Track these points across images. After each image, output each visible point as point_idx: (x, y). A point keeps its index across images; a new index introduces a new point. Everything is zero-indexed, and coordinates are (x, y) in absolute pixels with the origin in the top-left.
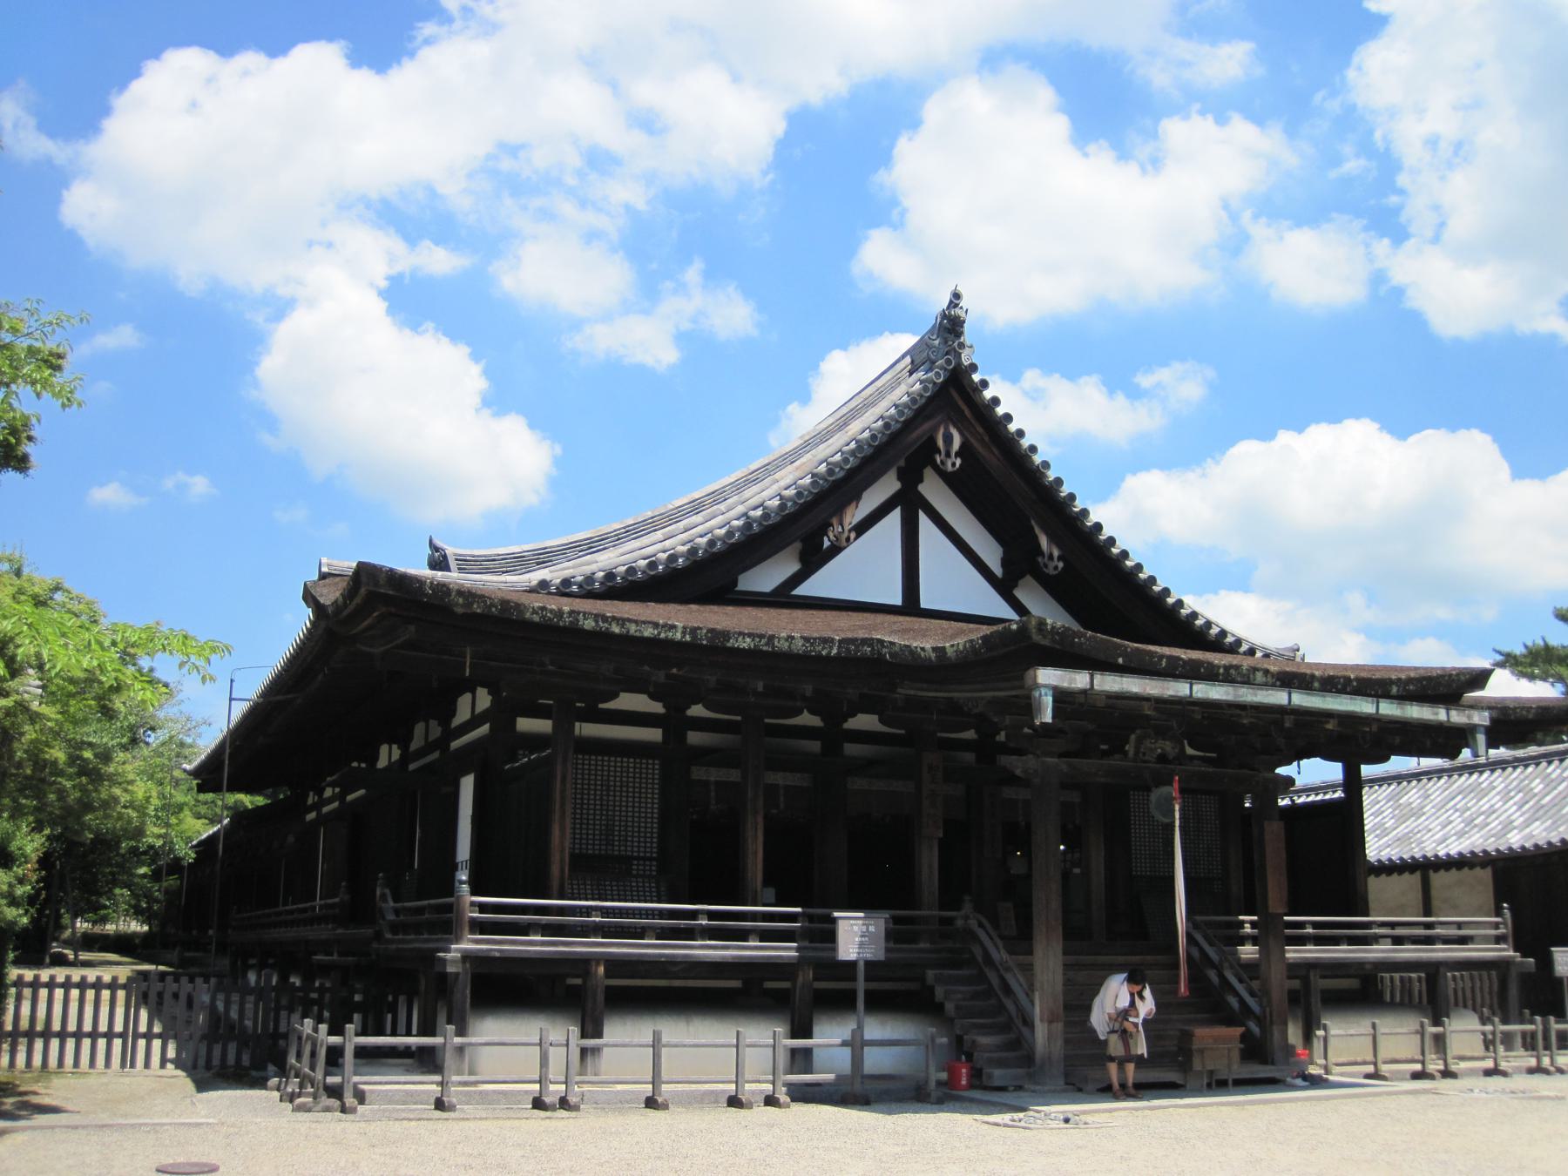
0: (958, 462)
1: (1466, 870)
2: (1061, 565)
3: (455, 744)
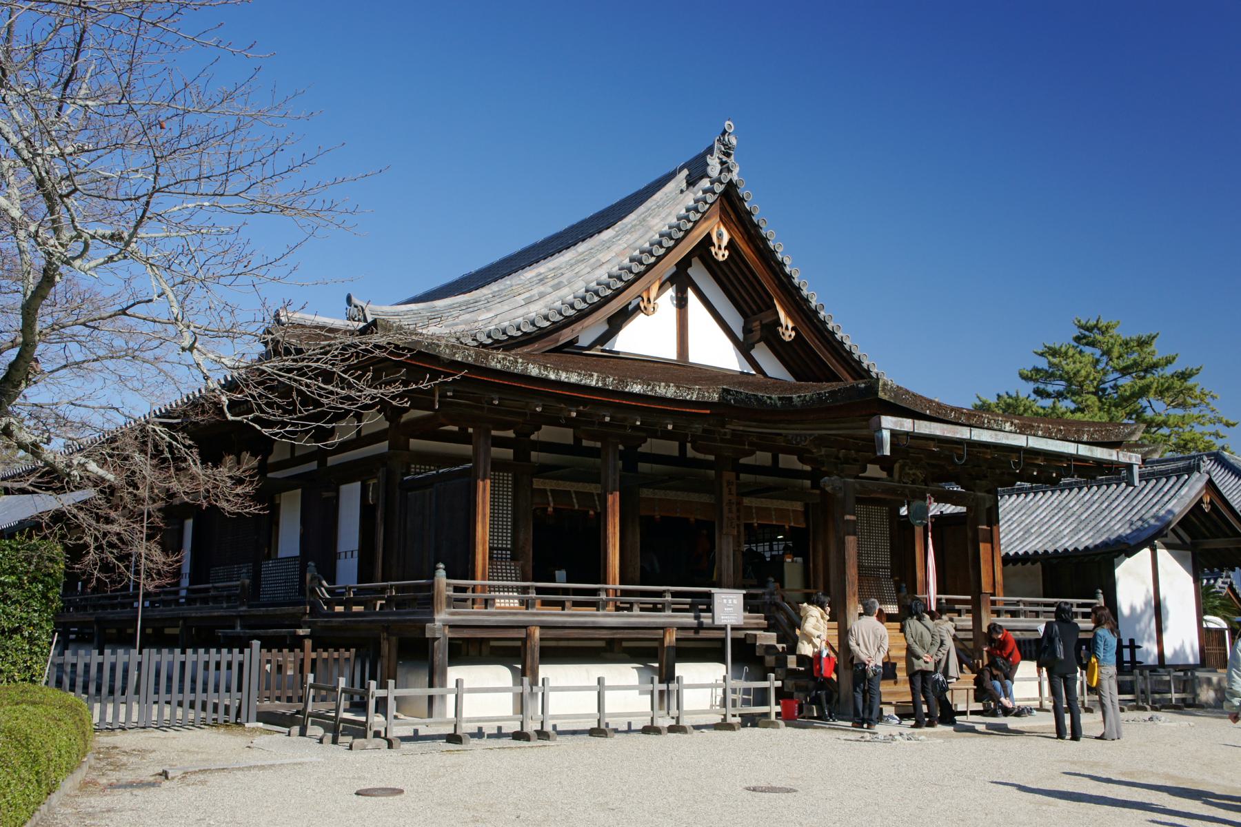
0: (727, 253)
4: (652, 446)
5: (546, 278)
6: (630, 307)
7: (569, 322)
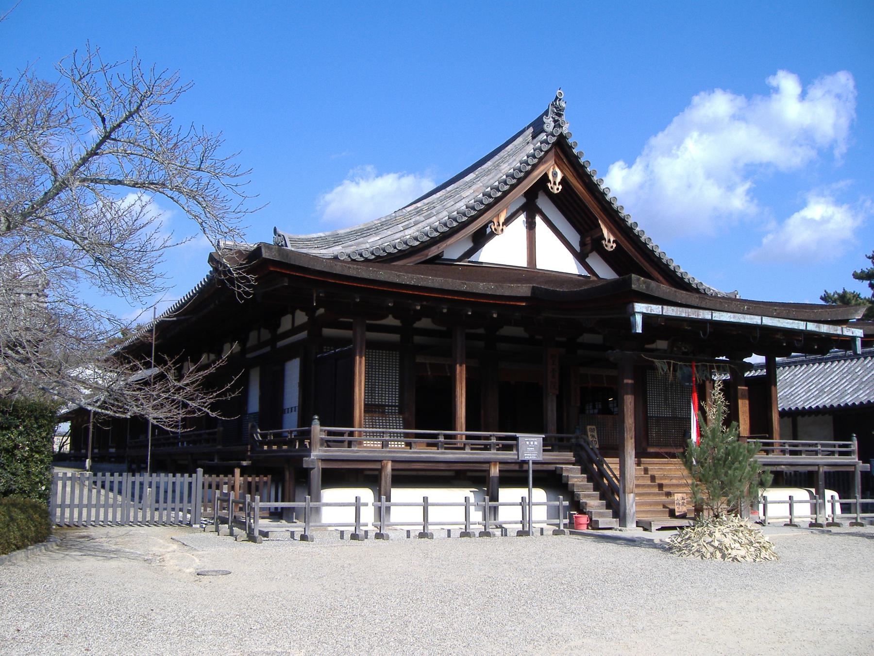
0: (560, 187)
1: (806, 417)
3: (281, 344)
4: (508, 331)
5: (422, 210)
6: (488, 230)
7: (434, 242)
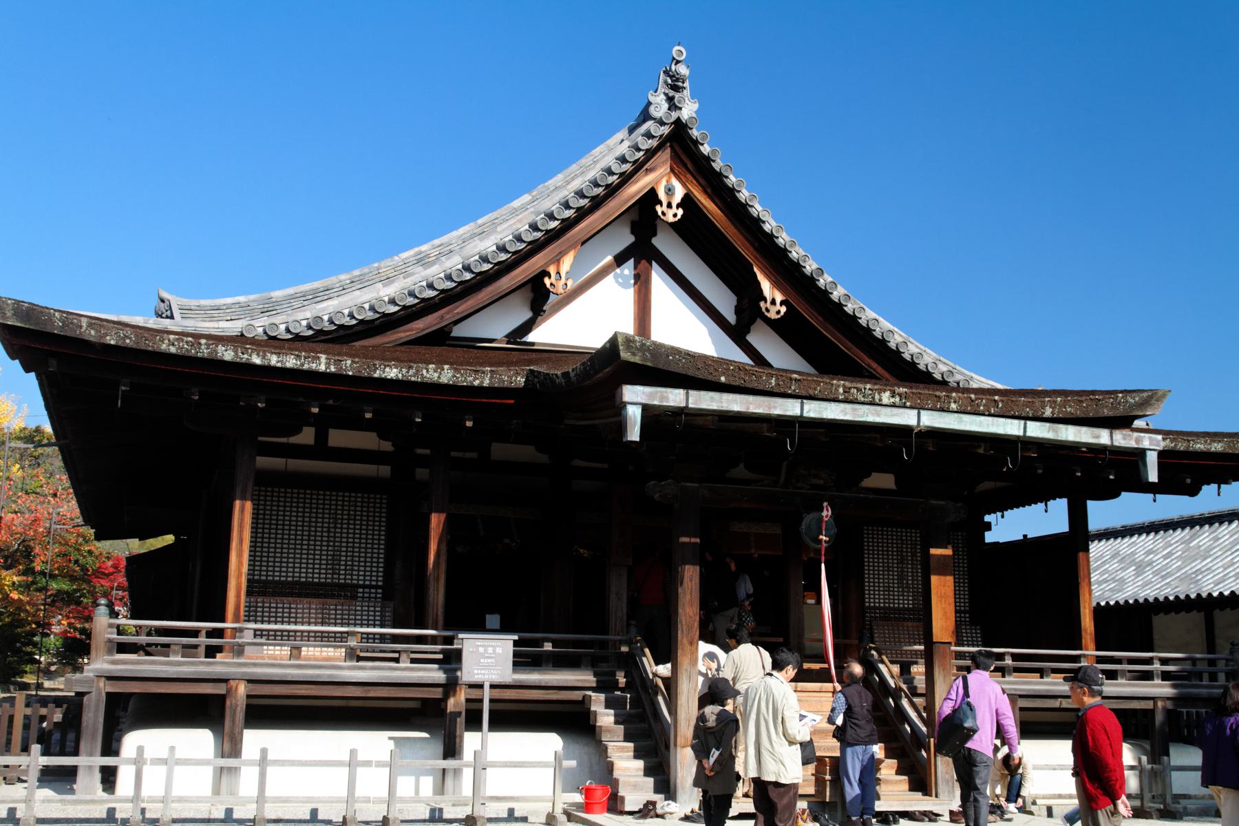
0: (680, 212)
2: (783, 309)
